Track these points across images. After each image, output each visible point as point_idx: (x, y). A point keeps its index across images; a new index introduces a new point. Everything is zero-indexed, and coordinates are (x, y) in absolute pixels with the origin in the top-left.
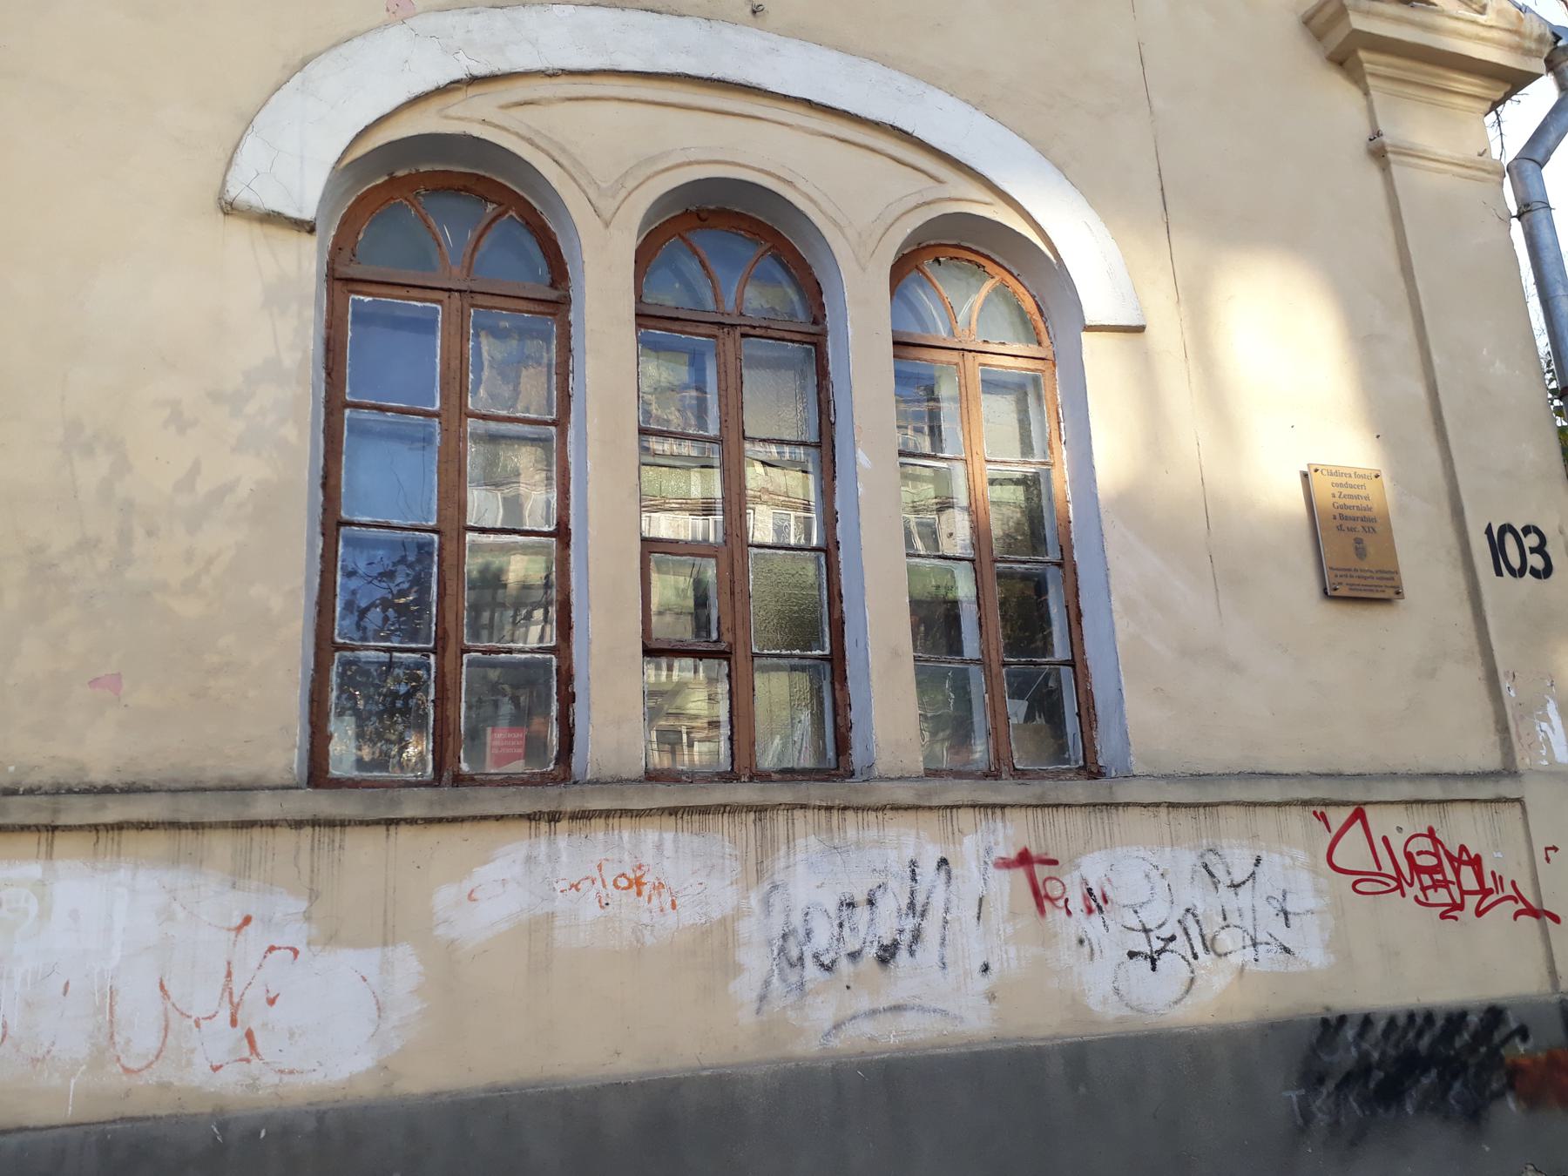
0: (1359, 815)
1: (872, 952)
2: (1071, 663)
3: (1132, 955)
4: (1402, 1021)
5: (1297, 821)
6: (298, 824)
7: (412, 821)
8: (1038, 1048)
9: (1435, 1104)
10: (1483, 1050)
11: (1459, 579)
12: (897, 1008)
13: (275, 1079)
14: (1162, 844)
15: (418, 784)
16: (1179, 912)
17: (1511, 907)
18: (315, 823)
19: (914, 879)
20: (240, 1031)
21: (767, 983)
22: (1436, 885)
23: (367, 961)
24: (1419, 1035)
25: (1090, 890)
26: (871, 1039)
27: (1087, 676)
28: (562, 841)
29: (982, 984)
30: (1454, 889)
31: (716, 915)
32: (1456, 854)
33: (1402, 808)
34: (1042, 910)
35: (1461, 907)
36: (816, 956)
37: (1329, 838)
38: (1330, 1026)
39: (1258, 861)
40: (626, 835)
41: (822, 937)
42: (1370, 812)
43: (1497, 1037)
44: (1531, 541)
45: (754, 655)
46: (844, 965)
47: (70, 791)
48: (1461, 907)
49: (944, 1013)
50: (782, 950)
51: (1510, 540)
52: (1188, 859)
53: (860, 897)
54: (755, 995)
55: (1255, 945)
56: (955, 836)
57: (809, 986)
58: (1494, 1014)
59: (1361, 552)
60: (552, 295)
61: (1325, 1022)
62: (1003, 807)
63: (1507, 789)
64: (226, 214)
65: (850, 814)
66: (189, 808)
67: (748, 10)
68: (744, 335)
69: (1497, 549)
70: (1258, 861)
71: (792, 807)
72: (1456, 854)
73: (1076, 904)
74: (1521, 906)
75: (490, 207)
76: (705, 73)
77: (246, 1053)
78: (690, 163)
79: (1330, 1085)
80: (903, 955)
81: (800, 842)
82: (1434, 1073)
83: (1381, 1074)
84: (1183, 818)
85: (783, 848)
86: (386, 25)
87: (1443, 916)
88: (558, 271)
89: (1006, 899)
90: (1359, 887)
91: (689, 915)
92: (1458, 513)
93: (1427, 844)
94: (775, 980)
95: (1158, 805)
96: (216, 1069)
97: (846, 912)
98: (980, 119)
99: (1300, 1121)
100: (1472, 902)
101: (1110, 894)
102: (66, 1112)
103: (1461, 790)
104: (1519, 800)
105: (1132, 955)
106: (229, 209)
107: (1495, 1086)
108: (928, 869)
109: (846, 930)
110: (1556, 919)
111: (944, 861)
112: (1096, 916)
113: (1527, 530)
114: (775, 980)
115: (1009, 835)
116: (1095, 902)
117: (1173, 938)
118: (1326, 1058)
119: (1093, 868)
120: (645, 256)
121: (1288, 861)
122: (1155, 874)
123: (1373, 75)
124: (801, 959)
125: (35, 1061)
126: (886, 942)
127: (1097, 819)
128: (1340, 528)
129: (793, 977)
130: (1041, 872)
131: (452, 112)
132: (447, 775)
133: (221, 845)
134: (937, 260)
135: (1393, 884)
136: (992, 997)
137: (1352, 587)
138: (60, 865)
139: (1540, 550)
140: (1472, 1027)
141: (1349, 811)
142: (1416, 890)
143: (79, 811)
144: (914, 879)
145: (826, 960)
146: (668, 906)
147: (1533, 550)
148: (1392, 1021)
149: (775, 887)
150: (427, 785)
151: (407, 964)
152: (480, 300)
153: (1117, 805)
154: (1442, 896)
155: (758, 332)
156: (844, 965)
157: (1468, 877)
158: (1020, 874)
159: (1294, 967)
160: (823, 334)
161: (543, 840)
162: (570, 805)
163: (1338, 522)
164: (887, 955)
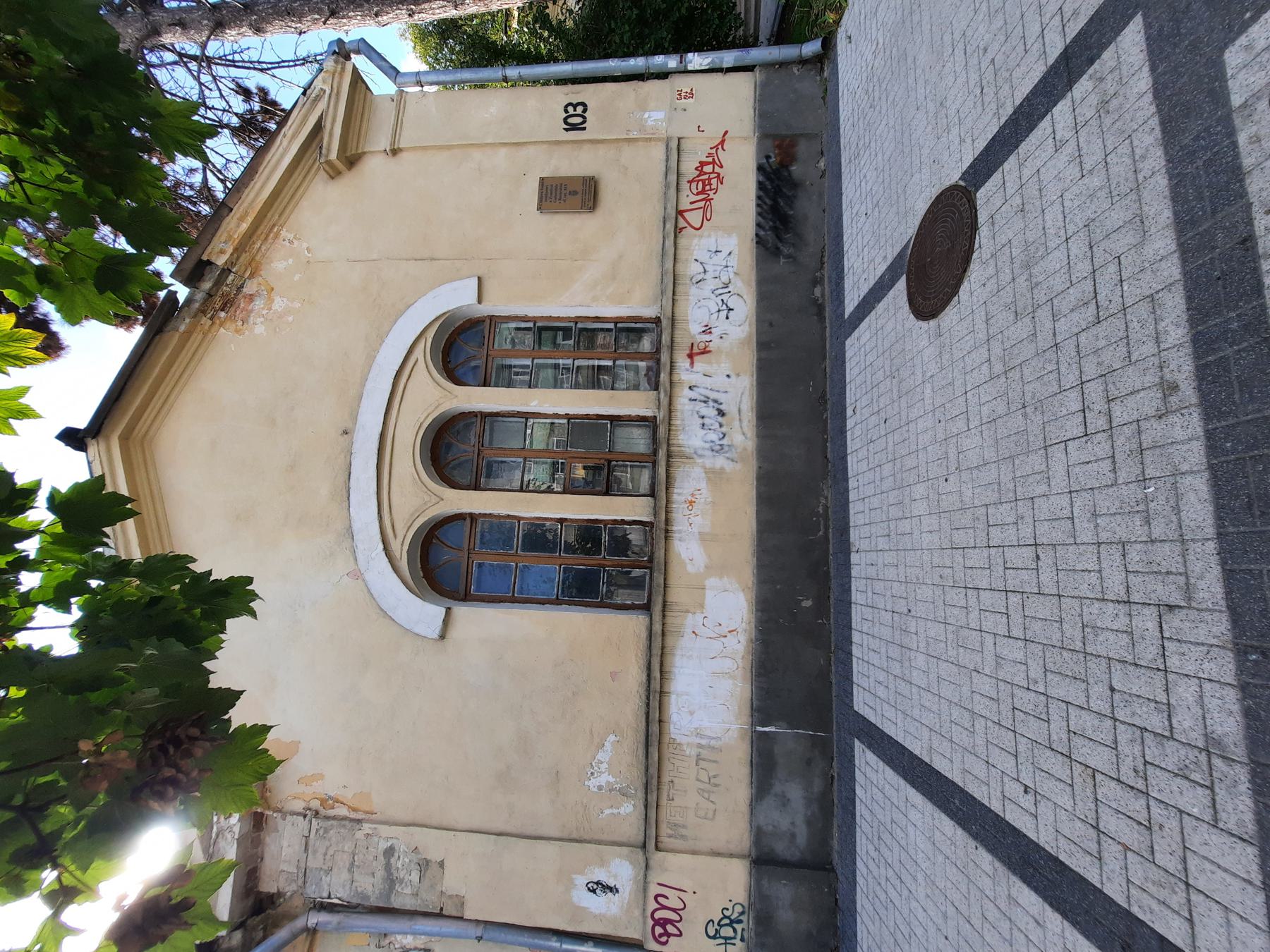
1: (720, 419)
2: (616, 323)
3: (727, 318)
4: (759, 210)
5: (682, 241)
6: (664, 616)
7: (665, 579)
8: (757, 360)
9: (790, 201)
10: (773, 176)
11: (586, 147)
12: (739, 411)
13: (744, 624)
14: (688, 300)
15: (651, 574)
16: (713, 296)
17: (720, 151)
18: (664, 611)
19: (696, 400)
20: (729, 635)
21: (728, 458)
22: (710, 184)
23: (709, 594)
24: (765, 203)
25: (703, 332)
26: (749, 421)
27: (621, 318)
28: (675, 528)
29: (733, 378)
30: (712, 176)
31: (704, 475)
32: (698, 172)
33: (680, 193)
34: (709, 352)
35: (719, 174)
36: (720, 439)
37: (689, 229)
38: (760, 241)
39: (696, 260)
40: (674, 506)
41: (713, 436)
42: (681, 208)
43: (769, 169)
44: (570, 109)
45: (609, 451)
46: (724, 429)
47: (649, 686)
48: (719, 174)
49: (742, 394)
50: (717, 452)
51: (571, 120)
52: (694, 290)
53: (701, 421)
54: (731, 463)
55: (727, 267)
56: (681, 382)
57: (730, 443)
58: (760, 168)
59: (574, 193)
60: (468, 520)
61: (757, 243)
62: (671, 362)
63: (674, 145)
64: (444, 638)
65: (672, 422)
66: (656, 651)
67: (346, 436)
68: (483, 446)
69: (573, 127)
70: (696, 260)
71: (669, 445)
72: (698, 172)
73: (707, 337)
74: (720, 147)
75: (434, 541)
76: (376, 456)
77: (735, 633)
78: (415, 464)
79: (780, 245)
80: (722, 407)
81: (680, 442)
82: (780, 200)
83: (778, 222)
84: (680, 289)
85: (682, 449)
86: (364, 580)
87: (722, 183)
88: (460, 517)
89: (704, 365)
90: (708, 218)
91: (703, 485)
92: (558, 143)
93: (694, 185)
94: (727, 455)
95: (673, 299)
96: (739, 642)
97: (706, 427)
98: (388, 341)
99: (791, 260)
100: (717, 169)
101: (705, 324)
102: (748, 686)
103: (674, 164)
104: (679, 139)
105: (727, 318)
106: (442, 636)
107: (786, 174)
108: (693, 394)
109: (712, 428)
110: (726, 132)
111: (690, 388)
112: (713, 330)
113: (566, 111)
114: (727, 455)
115: (682, 362)
116: (707, 330)
117: (722, 300)
118: (770, 245)
119: (695, 329)
120: (454, 485)
121: (697, 247)
122: (699, 304)
123: (357, 148)
124: (721, 445)
125: (732, 695)
126: (717, 413)
127: (678, 326)
128: (565, 201)
129: (726, 448)
130: (696, 350)
131: (398, 557)
132: (649, 565)
133: (670, 641)
134: (449, 362)
135: (708, 203)
136: (738, 375)
137: (589, 200)
138: (672, 689)
139: (575, 106)
140: (764, 180)
141: (679, 217)
142: (711, 193)
143: (656, 685)
144: (696, 400)
145: (722, 436)
146: (700, 492)
147: (575, 110)
148: (759, 214)
149: (695, 453)
150: (651, 571)
151: (711, 582)
152: (472, 546)
153: (673, 316)
154: (714, 182)
155: (481, 439)
156: (724, 429)
157: (708, 169)
158: (696, 358)
159: (736, 252)
160: (481, 413)
161: (674, 535)
162: (663, 525)
163: (562, 202)
164: (721, 413)
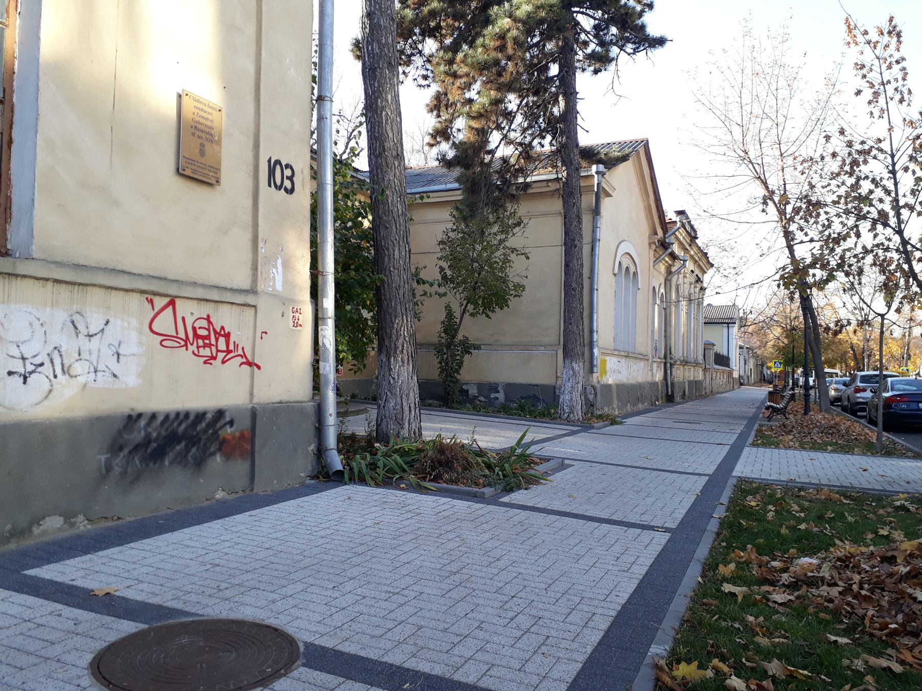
0: (172, 303)
42: (178, 302)
44: (288, 172)
52: (62, 316)
84: (63, 290)
103: (229, 297)
139: (291, 178)
